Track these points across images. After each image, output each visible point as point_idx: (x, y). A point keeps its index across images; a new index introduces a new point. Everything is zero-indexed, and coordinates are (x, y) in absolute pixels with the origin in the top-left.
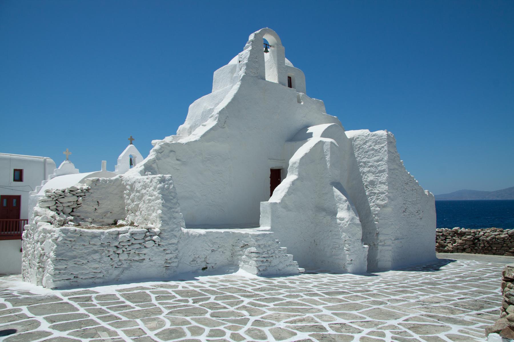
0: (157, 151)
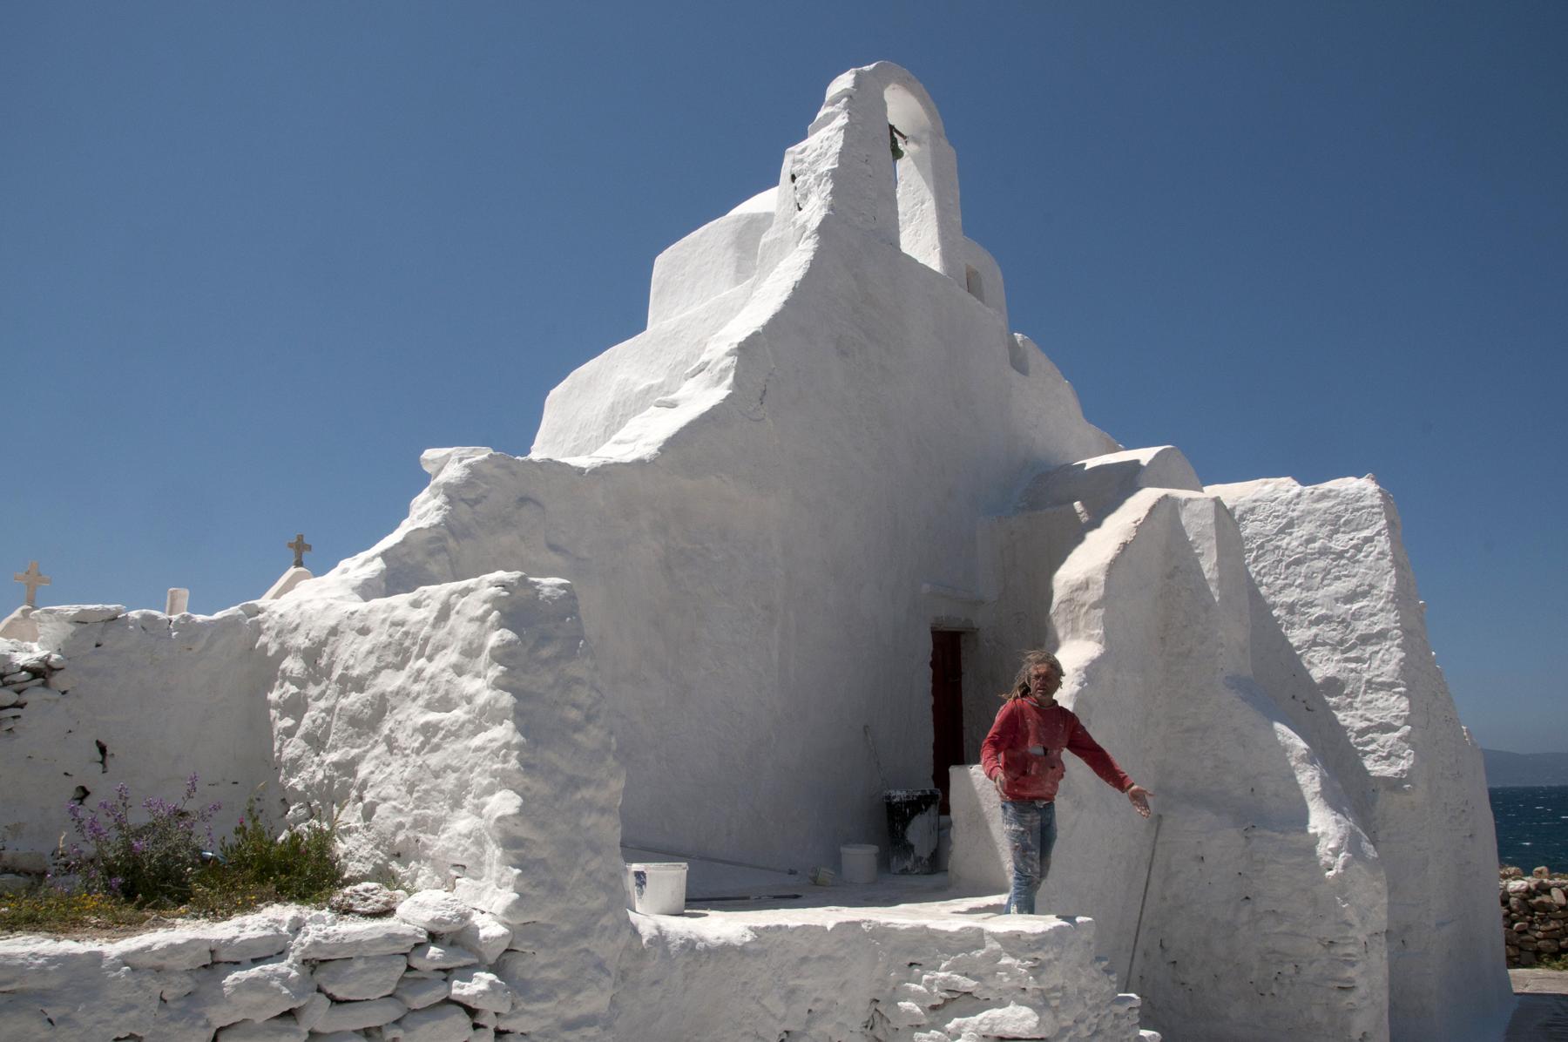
0: (453, 493)
